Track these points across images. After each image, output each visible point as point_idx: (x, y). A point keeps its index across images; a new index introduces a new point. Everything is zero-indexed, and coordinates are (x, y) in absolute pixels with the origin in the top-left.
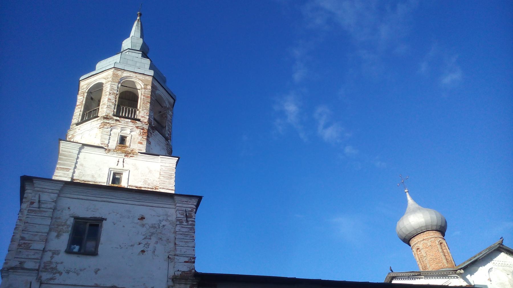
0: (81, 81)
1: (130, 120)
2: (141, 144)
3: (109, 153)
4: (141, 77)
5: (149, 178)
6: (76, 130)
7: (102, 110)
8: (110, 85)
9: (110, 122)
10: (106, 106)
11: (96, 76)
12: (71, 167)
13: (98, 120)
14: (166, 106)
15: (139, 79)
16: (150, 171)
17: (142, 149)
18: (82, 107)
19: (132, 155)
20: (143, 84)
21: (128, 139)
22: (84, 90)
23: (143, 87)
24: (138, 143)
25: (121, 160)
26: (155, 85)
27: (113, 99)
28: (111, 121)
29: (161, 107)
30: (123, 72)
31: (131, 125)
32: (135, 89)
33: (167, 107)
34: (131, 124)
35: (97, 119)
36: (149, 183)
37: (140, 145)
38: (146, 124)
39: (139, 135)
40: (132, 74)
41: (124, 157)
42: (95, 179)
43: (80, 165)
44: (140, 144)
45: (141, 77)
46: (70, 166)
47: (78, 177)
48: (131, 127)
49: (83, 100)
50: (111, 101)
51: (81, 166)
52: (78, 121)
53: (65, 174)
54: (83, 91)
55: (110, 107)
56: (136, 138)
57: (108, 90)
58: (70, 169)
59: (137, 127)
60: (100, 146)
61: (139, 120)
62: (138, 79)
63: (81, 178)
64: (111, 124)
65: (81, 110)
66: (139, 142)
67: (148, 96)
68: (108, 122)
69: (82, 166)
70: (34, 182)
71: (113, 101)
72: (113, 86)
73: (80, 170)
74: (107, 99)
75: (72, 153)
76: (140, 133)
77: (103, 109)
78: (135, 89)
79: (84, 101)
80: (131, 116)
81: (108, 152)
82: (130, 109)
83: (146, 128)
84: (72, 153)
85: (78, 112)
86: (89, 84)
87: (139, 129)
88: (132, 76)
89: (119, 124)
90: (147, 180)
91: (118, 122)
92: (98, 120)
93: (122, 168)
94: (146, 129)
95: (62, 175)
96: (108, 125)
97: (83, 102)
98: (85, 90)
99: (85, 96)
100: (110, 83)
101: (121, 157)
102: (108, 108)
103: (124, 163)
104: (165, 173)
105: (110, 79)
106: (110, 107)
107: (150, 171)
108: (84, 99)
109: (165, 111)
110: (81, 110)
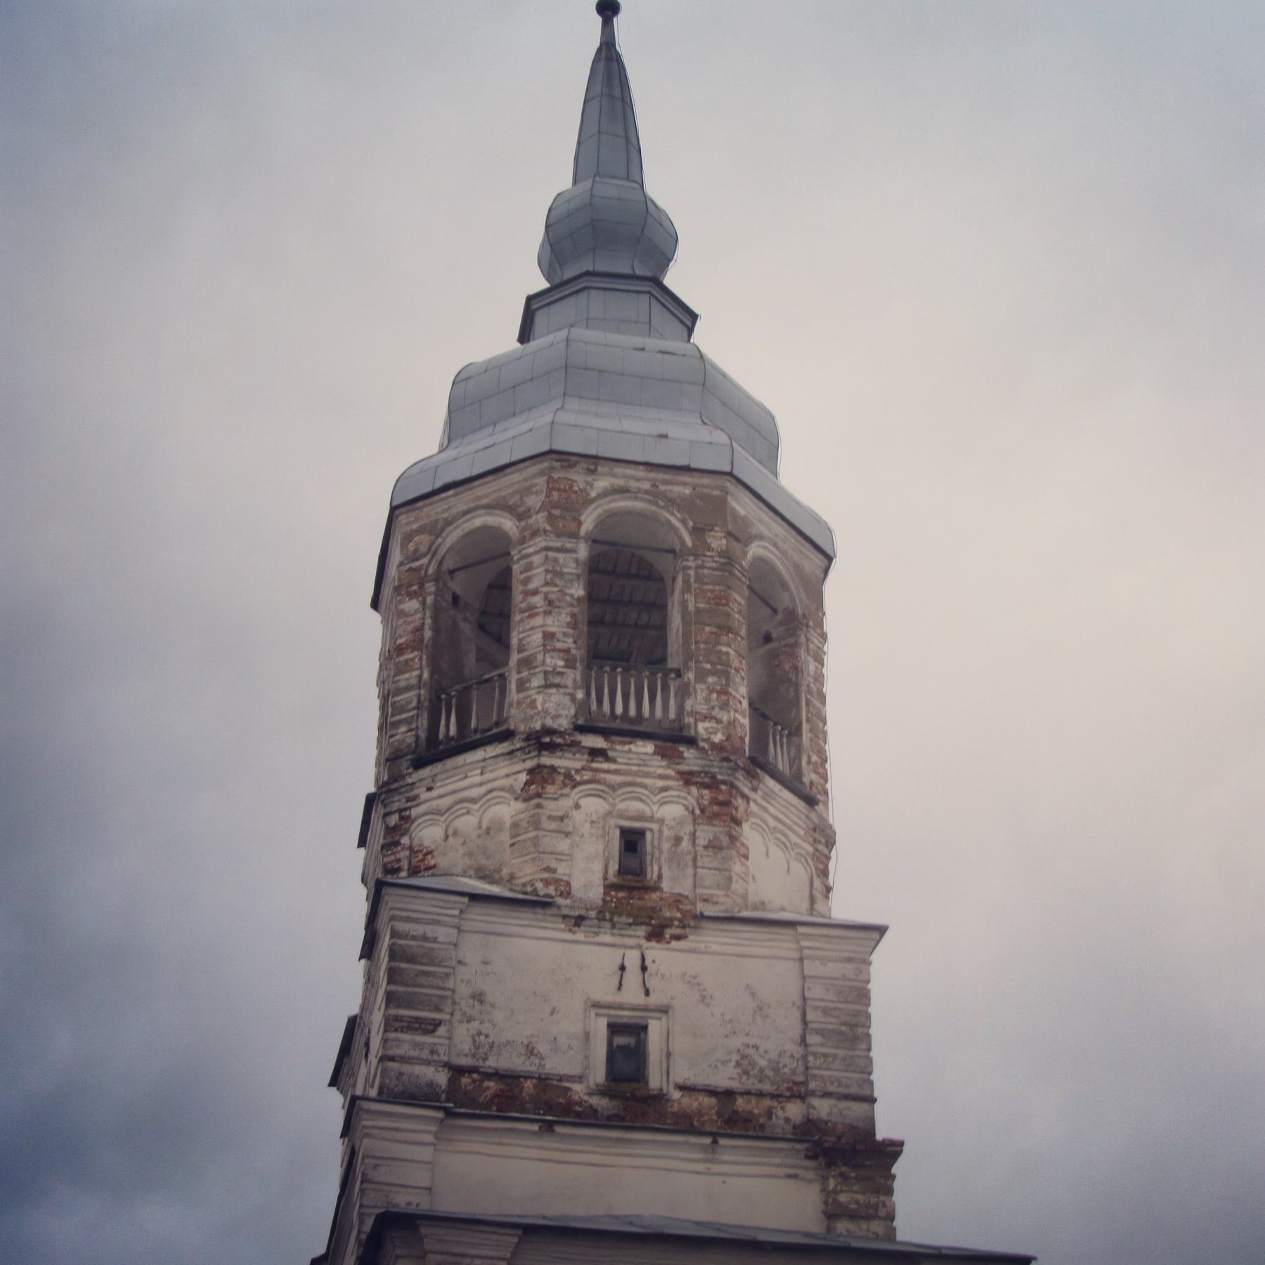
1: (649, 747)
6: (415, 792)
7: (522, 695)
22: (420, 562)
25: (632, 960)
26: (742, 512)
27: (565, 634)
29: (770, 612)
31: (660, 771)
35: (508, 750)
36: (762, 1070)
41: (643, 942)
42: (537, 1061)
43: (474, 997)
47: (474, 1056)
49: (423, 619)
50: (559, 645)
51: (476, 1003)
52: (418, 738)
59: (687, 778)
63: (485, 1059)
65: (420, 676)
69: (481, 1002)
70: (423, 1230)
71: (565, 646)
73: (476, 1024)
79: (426, 627)
87: (694, 790)
90: (751, 1051)
91: (600, 759)
93: (640, 999)
95: (413, 1053)
99: (430, 599)
101: (632, 942)
103: (647, 974)
106: (557, 680)
107: (761, 1009)
108: (428, 615)
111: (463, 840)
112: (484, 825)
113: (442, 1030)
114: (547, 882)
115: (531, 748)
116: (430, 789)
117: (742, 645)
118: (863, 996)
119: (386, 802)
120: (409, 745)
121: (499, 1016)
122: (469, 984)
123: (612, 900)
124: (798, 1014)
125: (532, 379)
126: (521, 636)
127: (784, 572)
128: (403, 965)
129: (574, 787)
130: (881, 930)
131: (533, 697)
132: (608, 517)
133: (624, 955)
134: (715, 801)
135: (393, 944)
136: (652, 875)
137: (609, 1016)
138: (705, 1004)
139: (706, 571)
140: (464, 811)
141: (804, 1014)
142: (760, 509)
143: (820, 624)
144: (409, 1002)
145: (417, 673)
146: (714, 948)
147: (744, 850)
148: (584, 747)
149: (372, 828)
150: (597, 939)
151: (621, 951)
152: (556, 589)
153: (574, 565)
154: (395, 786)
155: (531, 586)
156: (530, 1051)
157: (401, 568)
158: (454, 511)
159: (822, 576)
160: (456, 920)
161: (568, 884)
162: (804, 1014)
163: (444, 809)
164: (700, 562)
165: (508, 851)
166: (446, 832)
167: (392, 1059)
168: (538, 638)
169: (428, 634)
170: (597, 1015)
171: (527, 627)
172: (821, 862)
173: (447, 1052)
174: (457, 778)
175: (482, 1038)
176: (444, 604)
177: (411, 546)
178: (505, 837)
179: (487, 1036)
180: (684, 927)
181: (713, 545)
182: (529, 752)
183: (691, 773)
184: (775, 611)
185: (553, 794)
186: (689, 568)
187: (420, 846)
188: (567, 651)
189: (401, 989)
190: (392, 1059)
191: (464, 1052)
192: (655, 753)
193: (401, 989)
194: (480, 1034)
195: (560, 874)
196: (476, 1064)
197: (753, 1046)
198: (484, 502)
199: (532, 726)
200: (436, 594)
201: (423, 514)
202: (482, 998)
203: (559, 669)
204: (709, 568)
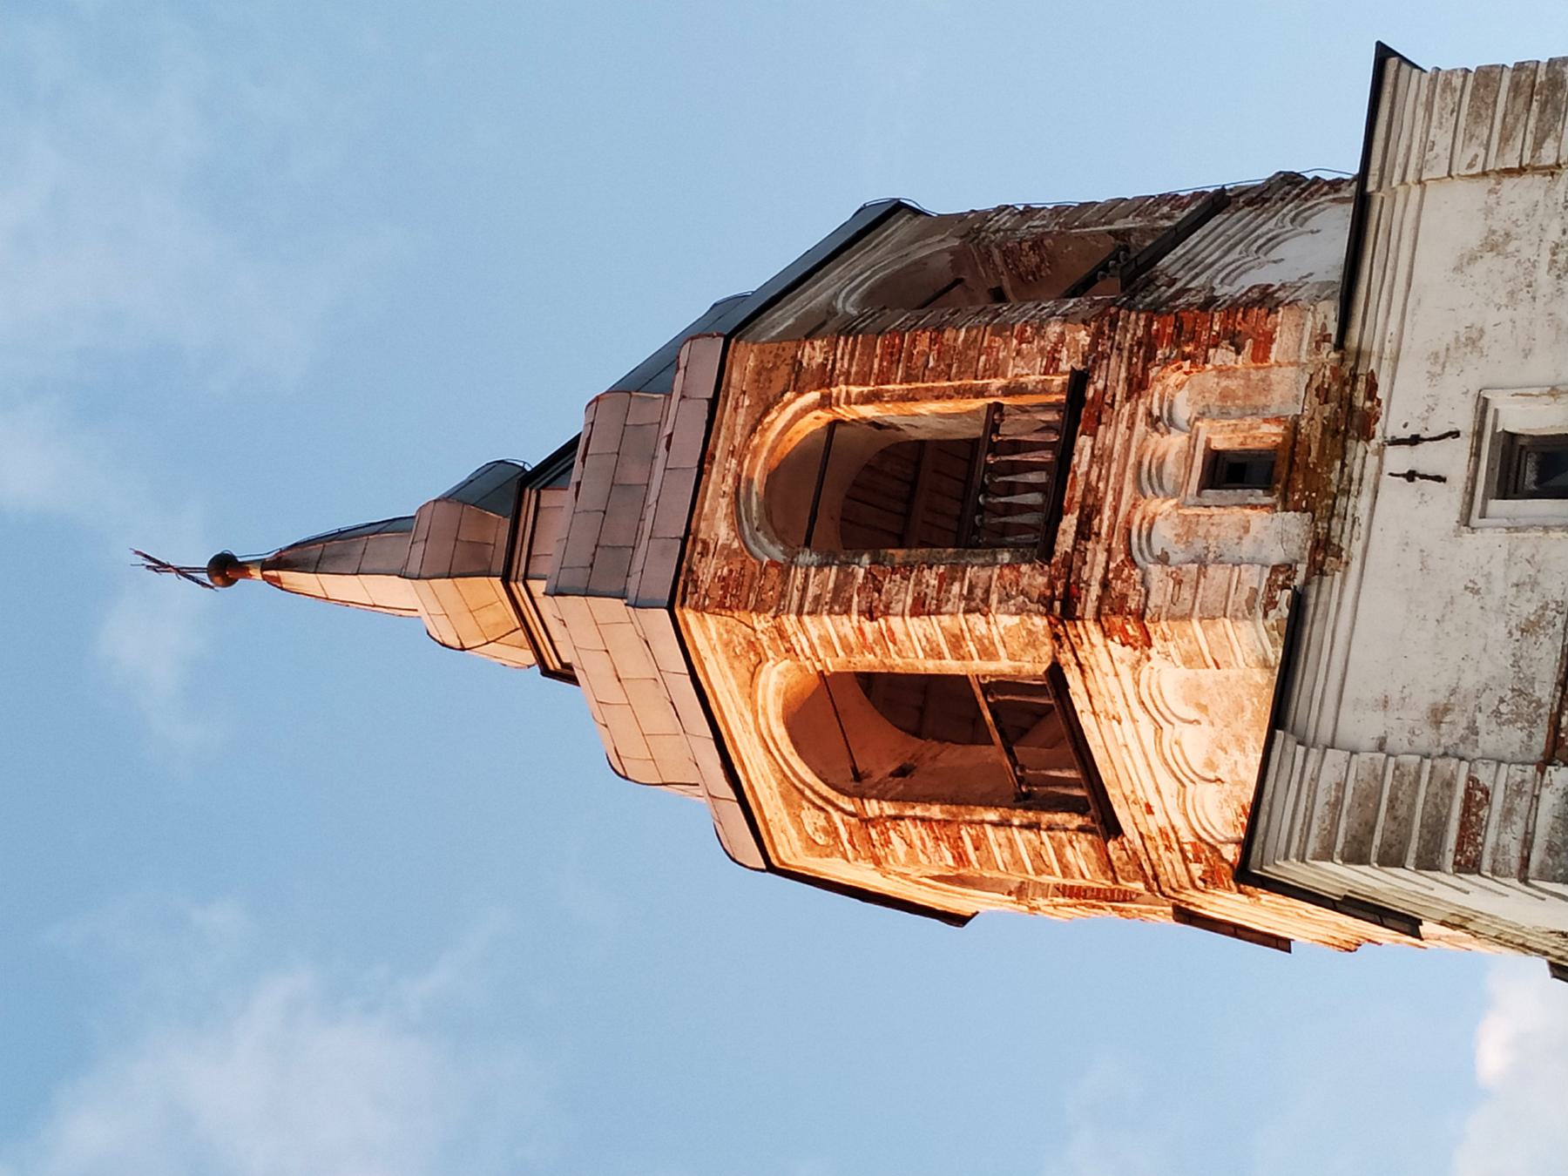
0: (771, 853)
1: (1084, 442)
2: (1272, 341)
3: (1344, 544)
4: (735, 419)
5: (1547, 245)
6: (1155, 833)
7: (1002, 652)
8: (806, 618)
9: (1098, 573)
10: (977, 620)
11: (735, 747)
12: (1453, 777)
13: (1079, 665)
14: (952, 251)
15: (754, 430)
16: (1494, 245)
17: (1309, 324)
18: (976, 818)
19: (1361, 386)
20: (788, 395)
21: (1224, 439)
23: (813, 396)
24: (1266, 358)
25: (1399, 458)
27: (918, 583)
28: (1086, 569)
30: (699, 549)
31: (1122, 427)
32: (825, 464)
33: (957, 242)
34: (1112, 435)
37: (1274, 347)
38: (1113, 325)
39: (1194, 364)
40: (719, 482)
42: (1550, 614)
43: (1438, 723)
44: (1267, 351)
45: (740, 420)
46: (1449, 785)
47: (1532, 723)
48: (1131, 428)
49: (914, 818)
50: (931, 592)
51: (1447, 719)
52: (1081, 829)
53: (1508, 813)
54: (844, 836)
55: (979, 592)
56: (1224, 383)
57: (847, 626)
58: (1473, 781)
59: (1137, 386)
60: (1286, 612)
61: (1079, 380)
62: (756, 440)
63: (1540, 705)
64: (1112, 565)
66: (1254, 358)
67: (883, 347)
68: (1095, 590)
69: (1447, 710)
71: (934, 582)
72: (817, 598)
73: (1481, 719)
74: (918, 626)
75: (1341, 787)
76: (1185, 359)
77: (993, 643)
78: (825, 464)
80: (1031, 488)
81: (1339, 557)
82: (990, 460)
83: (1142, 323)
84: (1341, 787)
85: (1011, 842)
86: (793, 792)
87: (1153, 373)
88: (730, 480)
89: (1116, 510)
92: (1079, 665)
93: (1464, 445)
94: (1148, 325)
95: (1518, 828)
96: (1118, 585)
97: (930, 820)
98: (836, 817)
99: (889, 809)
100: (789, 622)
101: (1372, 461)
102: (986, 600)
103: (1424, 435)
104: (1505, 139)
105: (762, 623)
106: (979, 592)
107: (1493, 248)
109: (989, 254)
110: (994, 824)
111: (1219, 751)
112: (1193, 714)
113: (1484, 776)
114: (1271, 603)
115: (1071, 632)
116: (1149, 809)
117: (987, 319)
118: (1487, 77)
119: (1175, 886)
120: (1092, 844)
121: (1470, 681)
122: (1417, 732)
123: (1306, 498)
124: (1508, 182)
125: (607, 651)
126: (921, 654)
127: (896, 267)
128: (1377, 841)
129: (1134, 563)
130: (1384, 54)
131: (1003, 632)
132: (771, 521)
133: (1391, 474)
134: (1176, 342)
135: (1342, 858)
136: (1275, 435)
137: (1485, 498)
138: (1481, 336)
139: (854, 370)
140: (1176, 749)
141: (1509, 172)
142: (793, 299)
143: (983, 216)
144: (1435, 830)
145: (988, 828)
146: (1393, 327)
147: (1256, 290)
148: (1074, 549)
149: (1274, 929)
150: (1364, 520)
151: (1385, 477)
152: (856, 599)
153: (826, 570)
154: (1149, 872)
155: (852, 638)
156: (1528, 629)
157: (850, 855)
158: (767, 770)
159: (922, 218)
160: (1314, 751)
161: (1275, 569)
162: (1509, 172)
163: (1176, 785)
164: (841, 378)
165: (1224, 671)
166: (1210, 781)
167: (1525, 862)
168: (920, 626)
169: (936, 812)
170: (1483, 516)
171: (908, 644)
172: (1321, 188)
173: (1520, 767)
174: (1128, 760)
175: (1503, 708)
176: (901, 787)
177: (821, 839)
178: (1209, 676)
179: (1502, 701)
180: (1355, 378)
181: (820, 360)
182: (1079, 636)
183: (1129, 381)
184: (958, 281)
185: (1140, 596)
186: (848, 393)
187: (1235, 826)
188: (941, 578)
189: (1414, 845)
190: (1525, 862)
191: (1525, 739)
192: (1094, 435)
193: (1414, 845)
194: (1497, 713)
195: (1260, 583)
196: (1546, 719)
197: (1554, 254)
198: (749, 718)
199: (1043, 632)
200: (879, 798)
201: (776, 819)
202: (1441, 708)
203: (965, 592)
204: (850, 365)
